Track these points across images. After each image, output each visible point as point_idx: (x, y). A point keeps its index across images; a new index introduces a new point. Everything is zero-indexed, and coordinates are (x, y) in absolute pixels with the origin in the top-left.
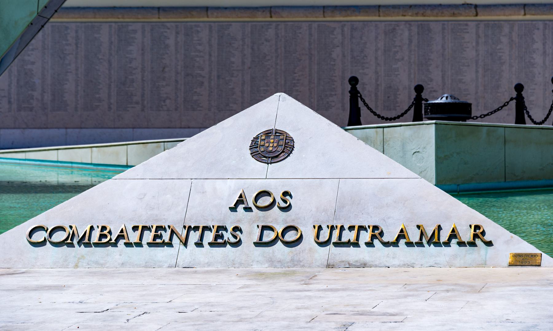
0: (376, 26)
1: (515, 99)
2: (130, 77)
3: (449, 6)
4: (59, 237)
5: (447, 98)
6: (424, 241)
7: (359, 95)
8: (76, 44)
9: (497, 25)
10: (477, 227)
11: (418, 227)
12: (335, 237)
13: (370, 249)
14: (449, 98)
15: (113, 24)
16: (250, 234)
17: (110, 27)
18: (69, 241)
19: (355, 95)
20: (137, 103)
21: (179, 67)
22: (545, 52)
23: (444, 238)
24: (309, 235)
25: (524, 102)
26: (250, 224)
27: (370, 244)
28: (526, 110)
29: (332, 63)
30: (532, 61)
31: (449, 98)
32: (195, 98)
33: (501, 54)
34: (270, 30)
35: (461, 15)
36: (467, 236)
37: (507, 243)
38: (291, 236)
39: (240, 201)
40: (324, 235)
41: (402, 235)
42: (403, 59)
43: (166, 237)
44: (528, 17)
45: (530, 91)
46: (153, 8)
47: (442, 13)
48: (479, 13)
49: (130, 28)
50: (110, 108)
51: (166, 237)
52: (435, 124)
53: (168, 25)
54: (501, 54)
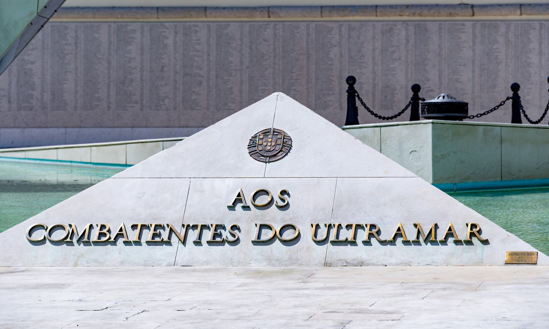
0: (373, 25)
1: (511, 98)
2: (129, 77)
3: (446, 6)
4: (59, 235)
5: (444, 97)
6: (421, 240)
7: (356, 94)
8: (76, 44)
9: (493, 25)
10: (473, 226)
11: (415, 225)
12: (332, 235)
13: (368, 247)
14: (446, 97)
15: (113, 24)
16: (248, 233)
17: (110, 26)
18: (68, 240)
19: (352, 94)
20: (136, 102)
21: (178, 67)
22: (541, 52)
23: (441, 236)
24: (307, 234)
25: (520, 101)
26: (248, 222)
27: (367, 243)
28: (522, 109)
29: (330, 63)
30: (528, 60)
31: (446, 97)
32: (194, 97)
33: (497, 54)
34: (268, 30)
35: (457, 15)
36: (464, 235)
37: (503, 242)
38: (289, 235)
39: (239, 199)
40: (322, 234)
41: (399, 233)
42: (400, 59)
43: (165, 235)
44: (524, 17)
45: (526, 90)
46: (152, 8)
47: (439, 13)
48: (476, 14)
49: (129, 28)
50: (109, 108)
51: (165, 235)
52: (432, 123)
53: (167, 24)
54: (497, 54)
